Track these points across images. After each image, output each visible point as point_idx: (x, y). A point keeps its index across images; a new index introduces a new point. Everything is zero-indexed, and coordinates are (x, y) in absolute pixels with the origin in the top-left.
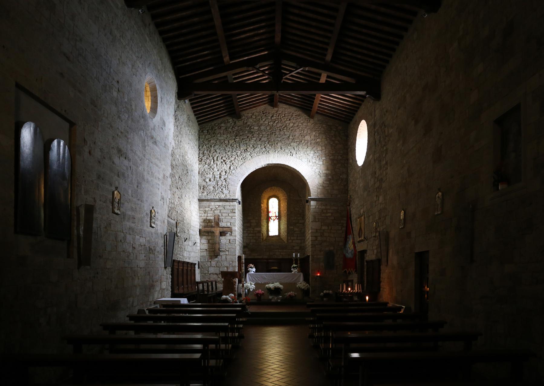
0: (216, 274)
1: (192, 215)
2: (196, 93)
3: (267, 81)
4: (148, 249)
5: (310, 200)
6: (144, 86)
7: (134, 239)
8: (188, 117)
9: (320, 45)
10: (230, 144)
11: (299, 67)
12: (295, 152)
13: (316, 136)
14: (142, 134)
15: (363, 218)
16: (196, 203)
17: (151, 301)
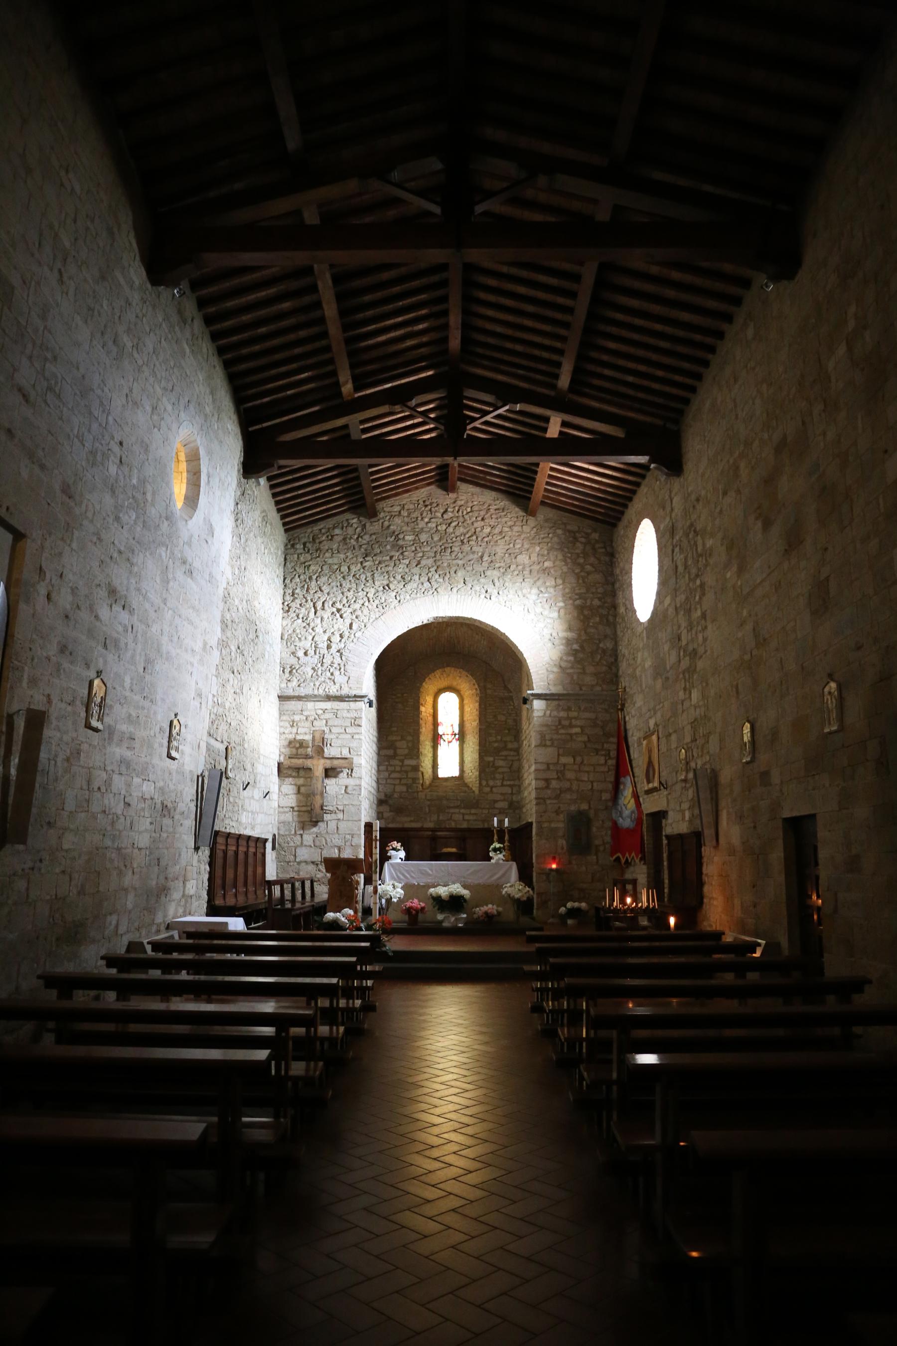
0: (313, 863)
1: (263, 732)
2: (282, 462)
3: (433, 435)
4: (159, 806)
5: (531, 698)
6: (175, 451)
7: (129, 785)
8: (264, 514)
9: (545, 355)
10: (352, 575)
11: (500, 404)
12: (496, 592)
13: (543, 555)
14: (164, 554)
15: (654, 738)
16: (272, 703)
17: (161, 923)
